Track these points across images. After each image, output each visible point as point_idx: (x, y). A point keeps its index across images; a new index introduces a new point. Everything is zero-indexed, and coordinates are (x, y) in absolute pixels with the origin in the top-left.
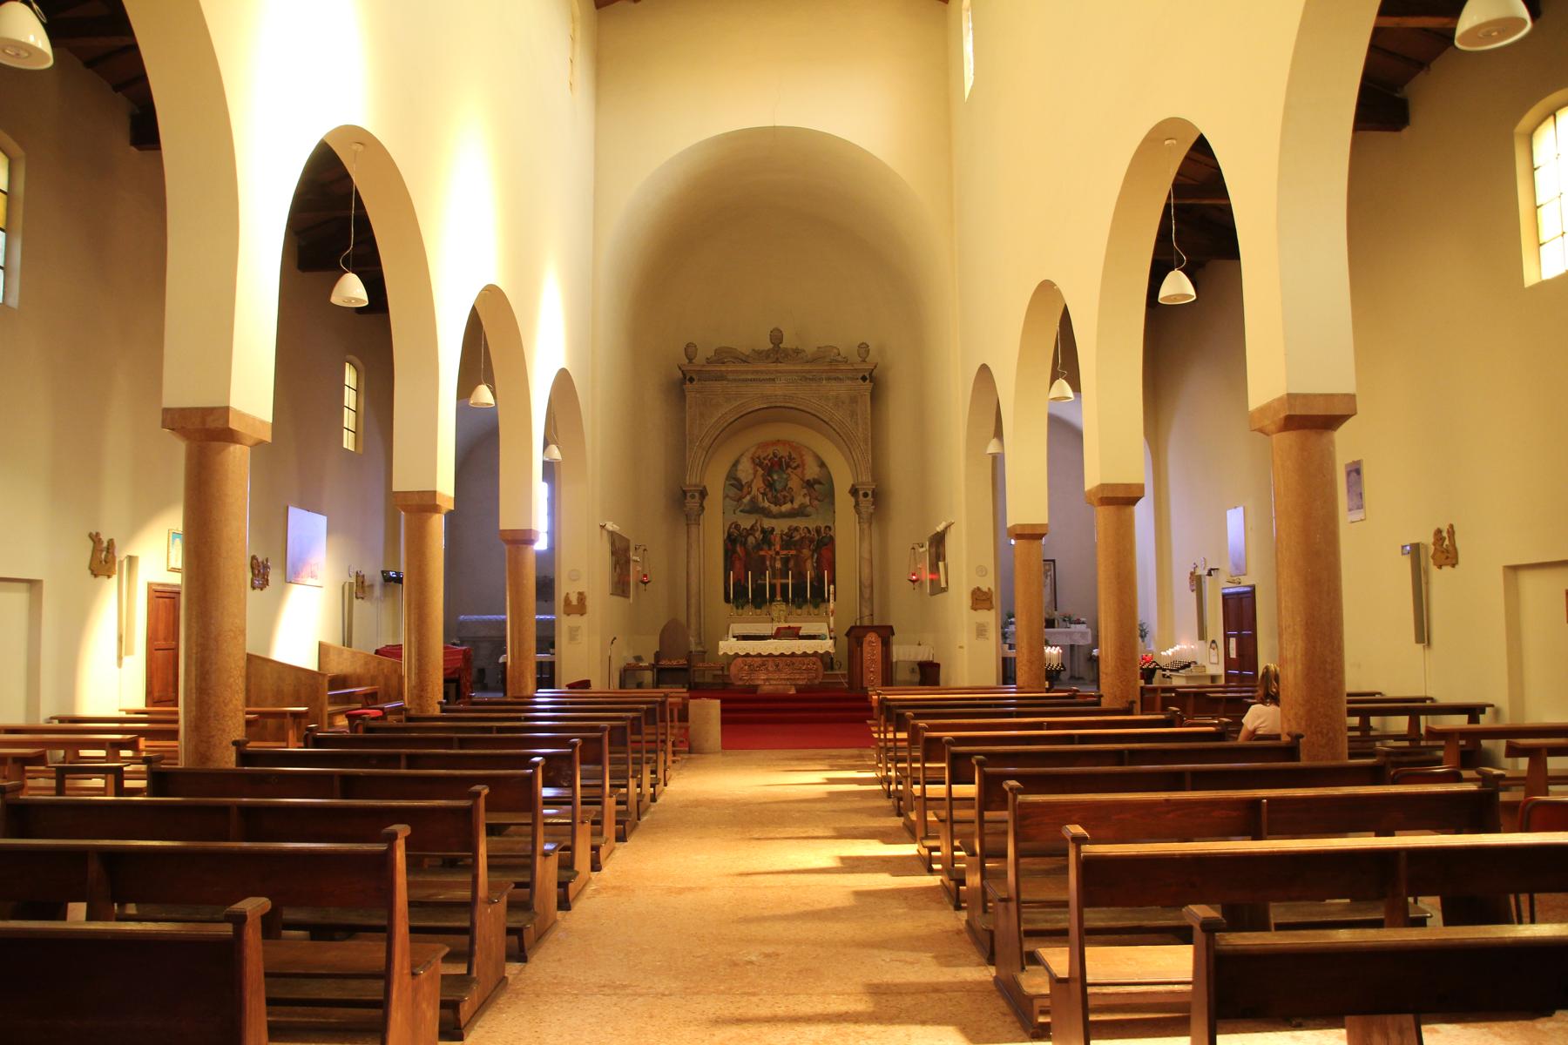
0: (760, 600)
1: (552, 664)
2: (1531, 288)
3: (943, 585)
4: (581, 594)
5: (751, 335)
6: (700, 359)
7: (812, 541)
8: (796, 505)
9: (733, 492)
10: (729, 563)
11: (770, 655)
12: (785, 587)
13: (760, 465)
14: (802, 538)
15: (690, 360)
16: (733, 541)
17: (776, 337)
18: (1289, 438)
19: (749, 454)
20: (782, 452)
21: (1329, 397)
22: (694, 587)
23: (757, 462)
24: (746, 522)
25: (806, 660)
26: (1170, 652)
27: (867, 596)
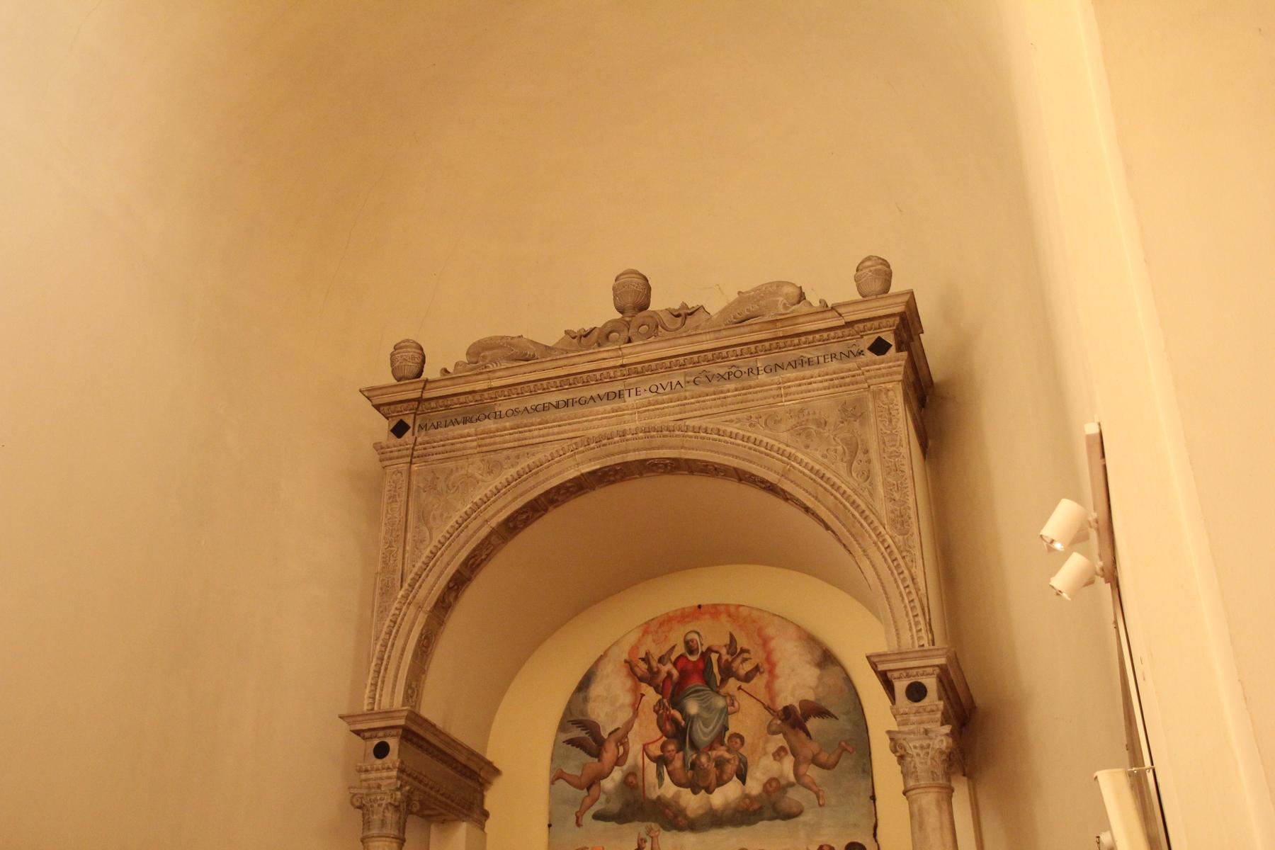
8: (754, 786)
9: (577, 762)
13: (651, 678)
20: (713, 636)
23: (642, 672)
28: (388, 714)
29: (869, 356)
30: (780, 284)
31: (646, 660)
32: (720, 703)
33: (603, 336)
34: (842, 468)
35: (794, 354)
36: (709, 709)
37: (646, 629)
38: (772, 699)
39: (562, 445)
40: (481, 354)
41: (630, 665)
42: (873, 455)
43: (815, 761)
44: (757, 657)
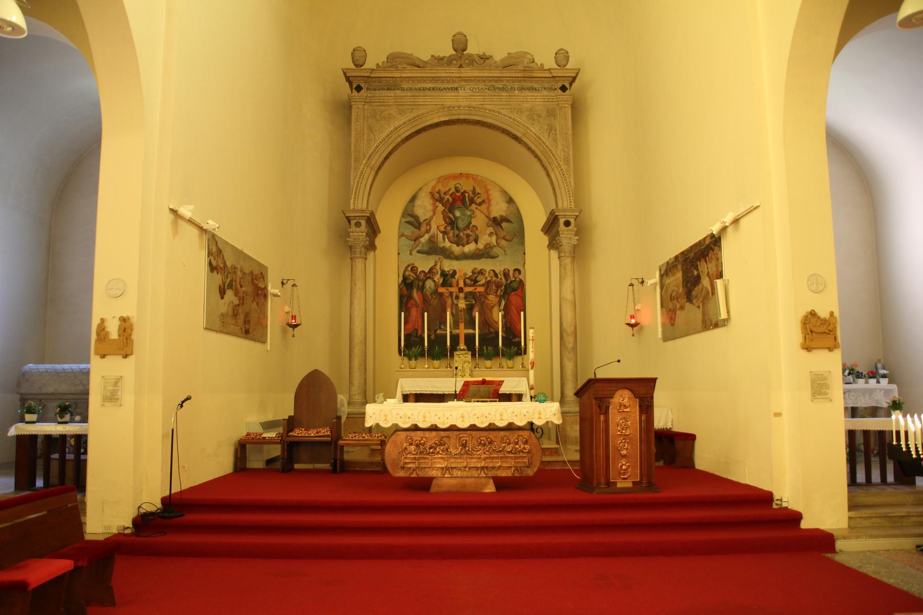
0: (439, 351)
1: (81, 441)
2: (176, 523)
3: (724, 315)
4: (124, 320)
5: (433, 44)
6: (370, 64)
7: (498, 286)
8: (481, 246)
9: (409, 230)
10: (405, 302)
11: (453, 428)
12: (470, 340)
13: (440, 200)
14: (488, 284)
15: (358, 66)
16: (409, 286)
19: (428, 189)
22: (358, 332)
23: (437, 198)
24: (424, 264)
25: (513, 436)
27: (570, 346)
28: (362, 211)
29: (560, 92)
30: (526, 53)
31: (439, 192)
32: (469, 213)
33: (449, 61)
34: (546, 135)
35: (529, 85)
36: (464, 215)
37: (439, 180)
38: (489, 213)
39: (433, 107)
40: (395, 60)
41: (432, 194)
42: (558, 132)
43: (504, 238)
44: (484, 197)
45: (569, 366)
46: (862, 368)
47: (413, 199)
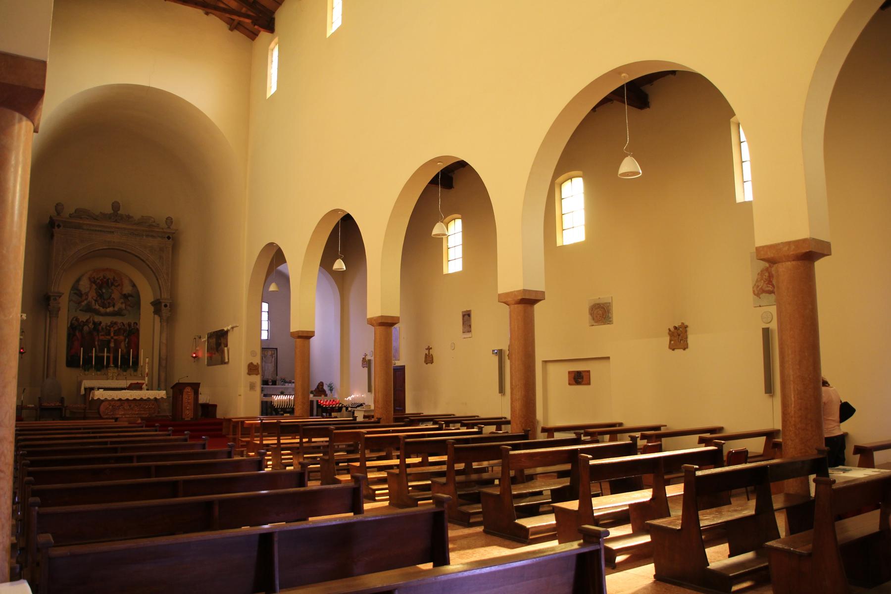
8: (116, 309)
13: (95, 282)
14: (119, 329)
15: (58, 214)
16: (74, 328)
17: (116, 206)
18: (521, 307)
21: (536, 292)
23: (92, 281)
24: (84, 317)
26: (350, 398)
41: (90, 279)
45: (163, 375)
46: (287, 380)
47: (78, 281)
